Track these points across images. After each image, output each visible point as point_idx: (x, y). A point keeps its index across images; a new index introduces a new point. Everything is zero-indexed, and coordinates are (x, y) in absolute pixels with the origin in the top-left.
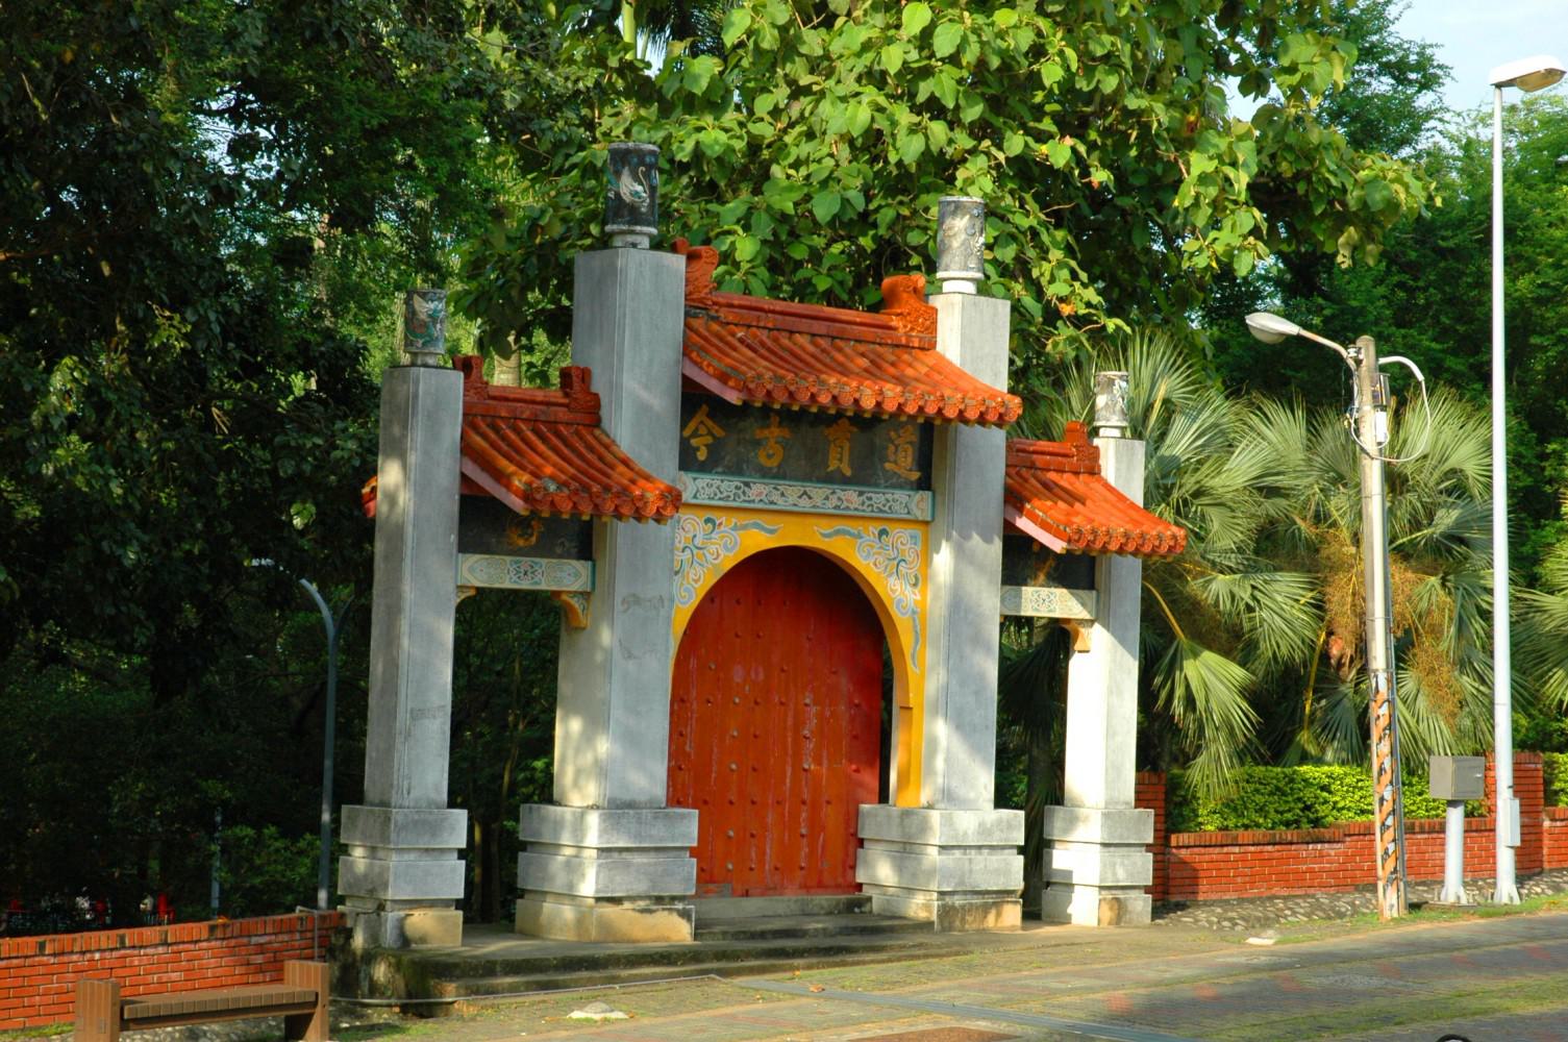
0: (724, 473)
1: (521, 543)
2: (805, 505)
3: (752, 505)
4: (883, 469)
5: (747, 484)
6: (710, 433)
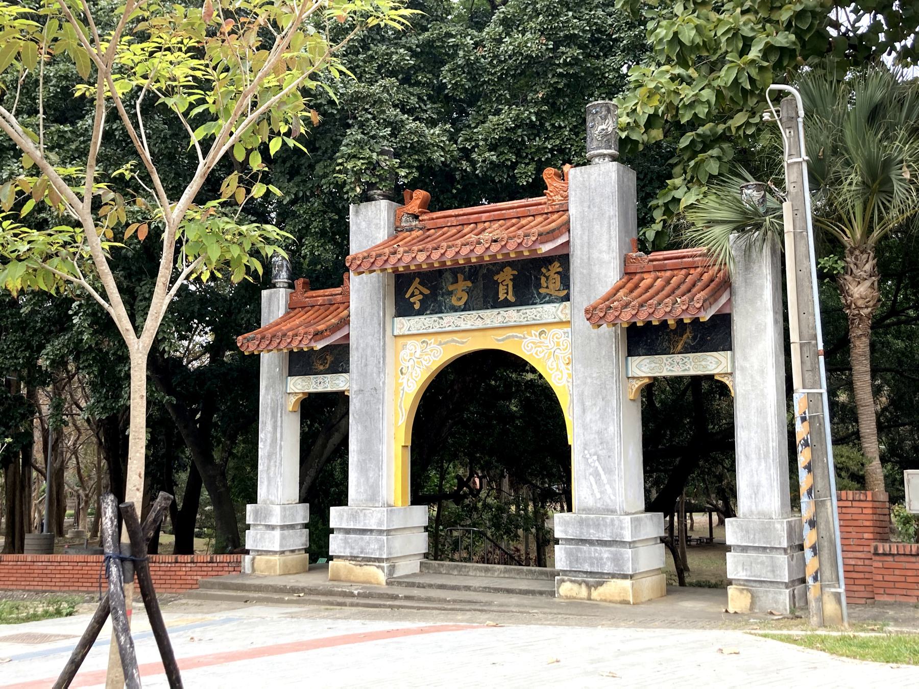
0: (431, 314)
1: (322, 368)
2: (479, 324)
3: (444, 330)
4: (539, 294)
5: (441, 318)
6: (421, 293)
